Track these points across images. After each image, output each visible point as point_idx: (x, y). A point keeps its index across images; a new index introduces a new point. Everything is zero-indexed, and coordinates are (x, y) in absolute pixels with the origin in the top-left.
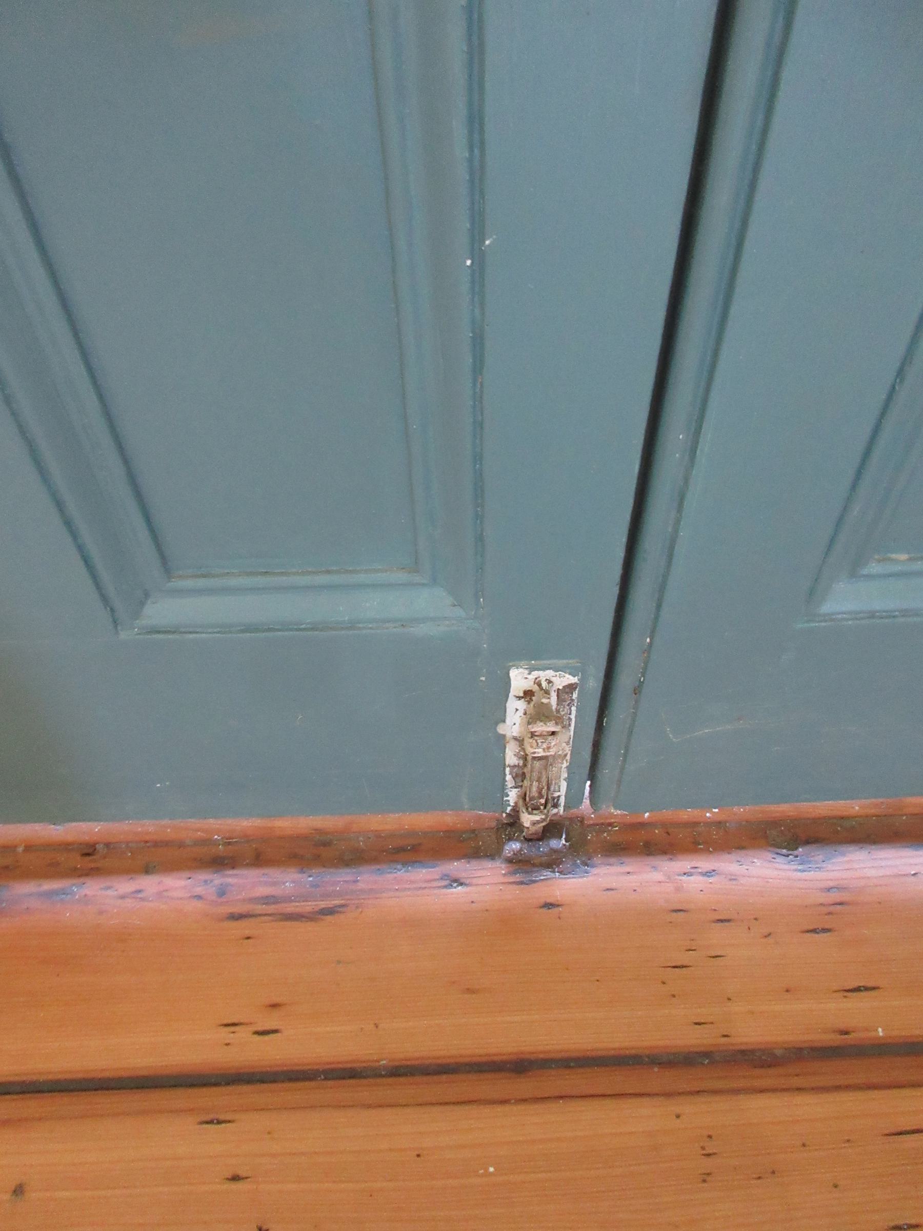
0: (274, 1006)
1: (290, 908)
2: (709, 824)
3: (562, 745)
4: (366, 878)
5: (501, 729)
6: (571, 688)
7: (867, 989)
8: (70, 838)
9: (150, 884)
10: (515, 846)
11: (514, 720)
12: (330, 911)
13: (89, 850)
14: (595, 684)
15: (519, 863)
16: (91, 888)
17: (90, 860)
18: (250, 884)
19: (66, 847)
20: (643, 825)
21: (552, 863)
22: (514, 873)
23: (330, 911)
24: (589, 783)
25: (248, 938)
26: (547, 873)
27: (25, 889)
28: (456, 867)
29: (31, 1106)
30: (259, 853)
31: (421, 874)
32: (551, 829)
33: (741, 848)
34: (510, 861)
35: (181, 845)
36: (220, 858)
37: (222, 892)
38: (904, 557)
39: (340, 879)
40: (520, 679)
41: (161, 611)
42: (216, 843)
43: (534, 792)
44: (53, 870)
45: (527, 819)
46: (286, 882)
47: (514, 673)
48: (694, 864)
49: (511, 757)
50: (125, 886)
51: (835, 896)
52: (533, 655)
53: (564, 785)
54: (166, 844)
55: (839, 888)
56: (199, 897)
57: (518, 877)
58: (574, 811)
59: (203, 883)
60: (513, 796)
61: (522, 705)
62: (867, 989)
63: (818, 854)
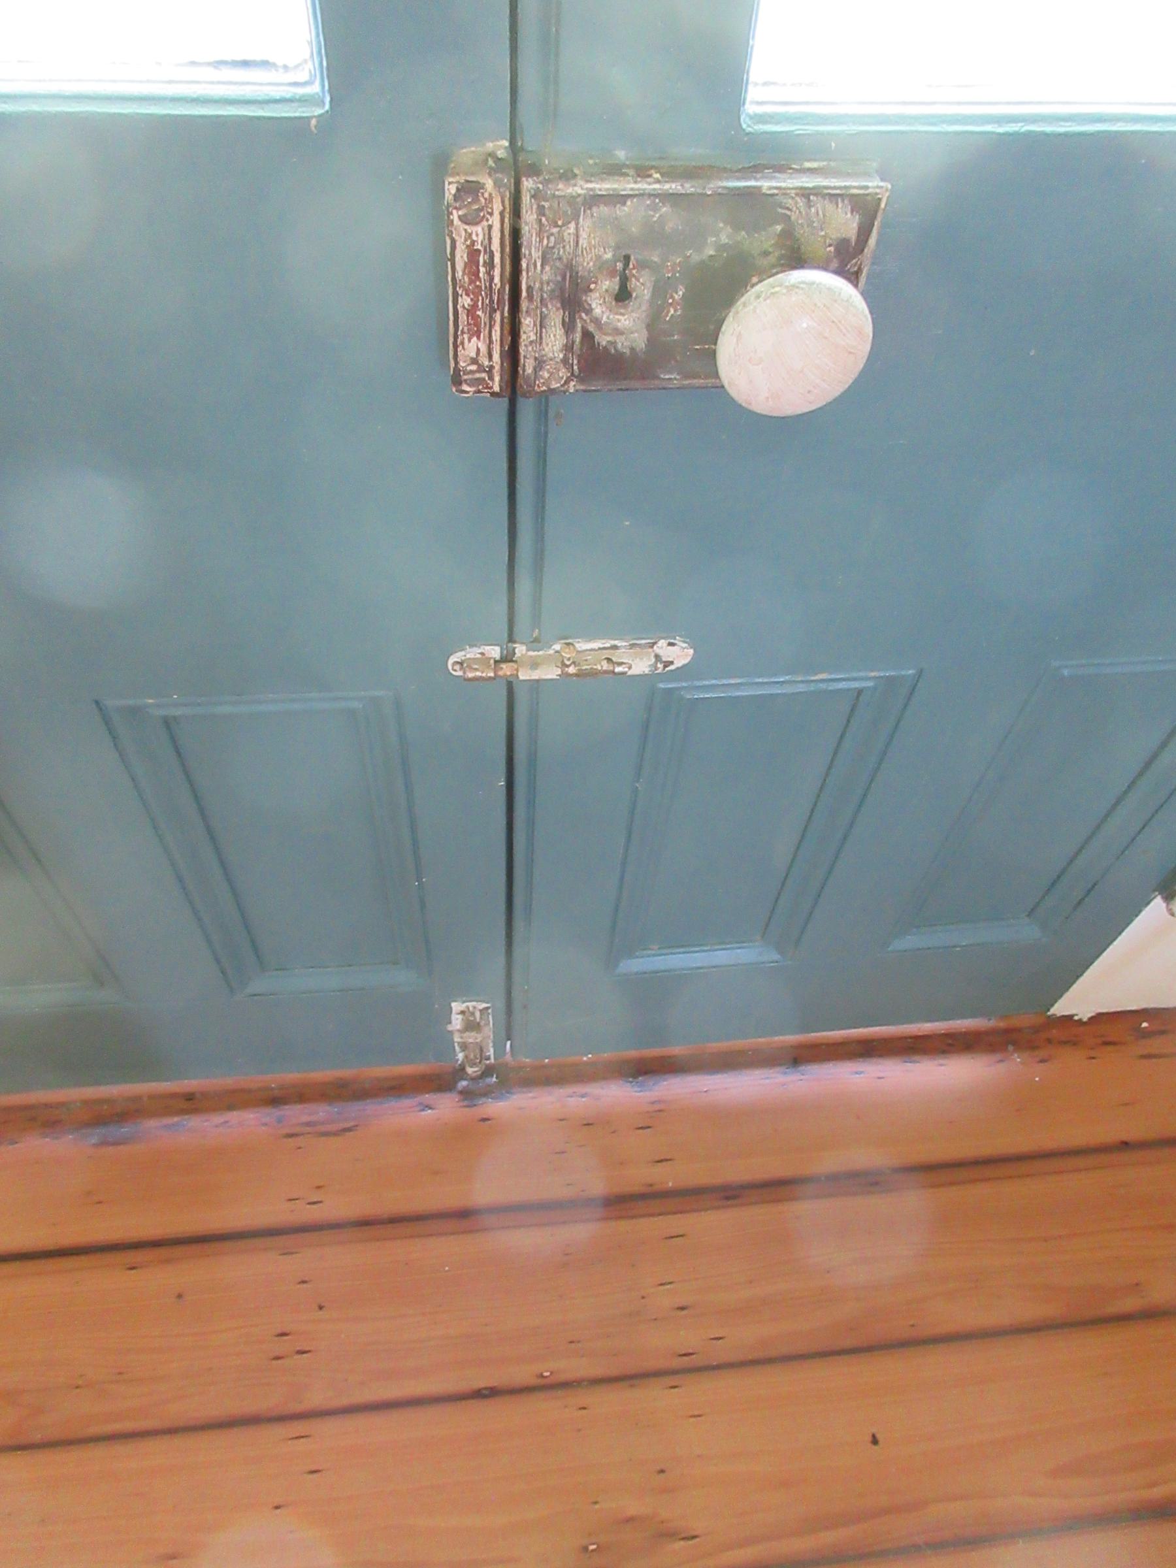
0: (319, 1187)
1: (322, 1128)
2: (586, 1063)
3: (487, 1036)
4: (369, 1107)
5: (450, 1028)
6: (487, 1008)
7: (667, 1160)
8: (178, 1090)
9: (234, 1116)
10: (464, 1083)
11: (457, 1022)
12: (349, 1130)
13: (189, 1097)
14: (501, 1004)
15: (466, 1094)
16: (194, 1122)
17: (191, 1103)
18: (296, 1114)
19: (174, 1096)
20: (544, 1066)
21: (487, 1093)
22: (463, 1100)
23: (349, 1130)
24: (509, 1043)
25: (682, 1308)
26: (484, 1099)
27: (152, 1124)
28: (428, 1098)
29: (179, 1251)
30: (301, 1095)
31: (407, 1102)
32: (488, 1071)
33: (605, 1078)
34: (461, 1092)
35: (250, 1091)
36: (275, 1100)
37: (279, 1121)
38: (656, 947)
39: (354, 1109)
40: (456, 1006)
41: (258, 985)
42: (272, 1089)
43: (472, 1056)
44: (168, 1111)
45: (470, 1070)
46: (321, 1112)
47: (453, 1004)
48: (575, 1090)
49: (457, 1039)
50: (217, 1119)
51: (657, 1107)
52: (465, 993)
53: (492, 1050)
54: (243, 1091)
55: (659, 1101)
56: (265, 1124)
57: (466, 1103)
58: (501, 1060)
59: (268, 1115)
60: (461, 1056)
61: (460, 1017)
62: (667, 1160)
63: (650, 1081)
